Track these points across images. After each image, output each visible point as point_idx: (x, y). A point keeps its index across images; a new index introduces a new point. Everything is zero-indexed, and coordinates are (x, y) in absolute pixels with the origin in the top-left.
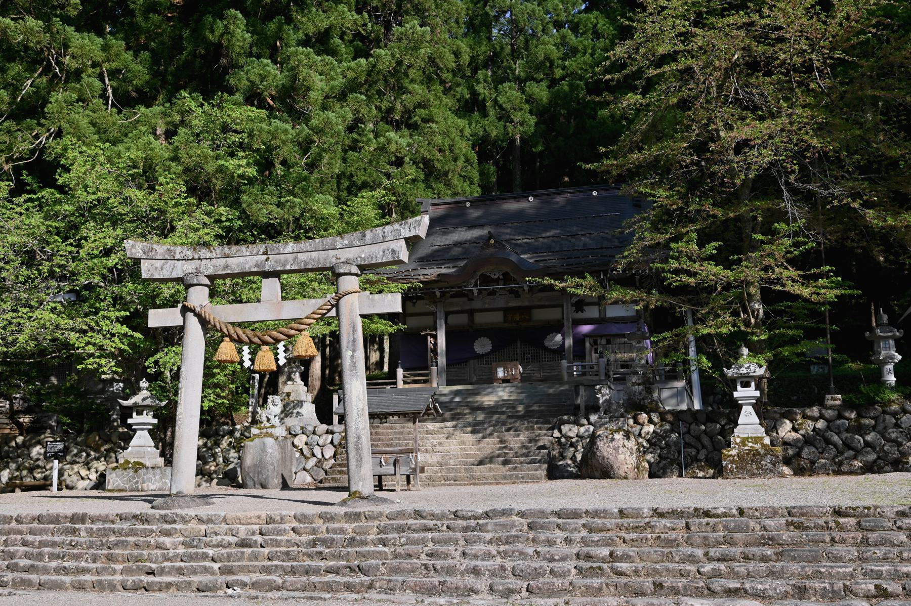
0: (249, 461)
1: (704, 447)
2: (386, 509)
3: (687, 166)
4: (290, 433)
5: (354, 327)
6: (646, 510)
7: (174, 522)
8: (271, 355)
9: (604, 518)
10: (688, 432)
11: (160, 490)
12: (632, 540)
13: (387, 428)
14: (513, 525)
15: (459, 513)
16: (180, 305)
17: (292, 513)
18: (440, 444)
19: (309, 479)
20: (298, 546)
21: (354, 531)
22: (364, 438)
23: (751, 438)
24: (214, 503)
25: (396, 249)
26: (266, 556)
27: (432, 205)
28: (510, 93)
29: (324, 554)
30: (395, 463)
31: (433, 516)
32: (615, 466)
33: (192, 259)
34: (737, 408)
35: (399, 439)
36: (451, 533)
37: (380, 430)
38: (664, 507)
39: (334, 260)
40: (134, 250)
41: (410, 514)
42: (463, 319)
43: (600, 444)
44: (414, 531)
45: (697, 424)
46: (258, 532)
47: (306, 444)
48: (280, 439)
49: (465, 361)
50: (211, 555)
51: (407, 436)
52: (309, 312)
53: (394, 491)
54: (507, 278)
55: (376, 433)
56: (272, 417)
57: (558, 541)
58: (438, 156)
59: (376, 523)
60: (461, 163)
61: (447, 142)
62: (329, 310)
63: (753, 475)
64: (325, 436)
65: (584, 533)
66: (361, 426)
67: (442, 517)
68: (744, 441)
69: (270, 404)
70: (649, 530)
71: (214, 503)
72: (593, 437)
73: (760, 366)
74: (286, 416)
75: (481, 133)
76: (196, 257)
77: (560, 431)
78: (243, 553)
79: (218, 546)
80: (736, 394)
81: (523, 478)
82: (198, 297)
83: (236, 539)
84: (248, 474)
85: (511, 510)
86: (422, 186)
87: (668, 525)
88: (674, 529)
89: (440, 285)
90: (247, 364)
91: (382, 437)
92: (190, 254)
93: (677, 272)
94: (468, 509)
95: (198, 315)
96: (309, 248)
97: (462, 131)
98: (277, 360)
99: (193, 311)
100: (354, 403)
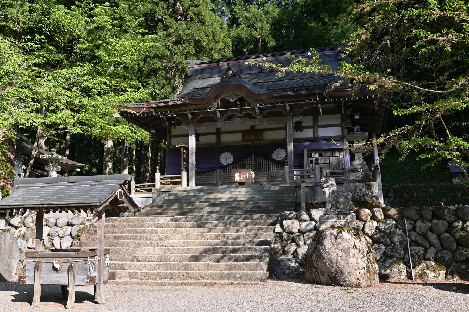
1: (431, 245)
10: (414, 229)
13: (124, 221)
27: (196, 64)
30: (70, 268)
32: (346, 272)
42: (212, 139)
43: (327, 242)
45: (422, 221)
49: (213, 170)
54: (242, 101)
55: (112, 225)
58: (205, 39)
61: (211, 30)
64: (64, 228)
72: (319, 238)
77: (282, 226)
89: (191, 107)
91: (116, 230)
93: (438, 25)
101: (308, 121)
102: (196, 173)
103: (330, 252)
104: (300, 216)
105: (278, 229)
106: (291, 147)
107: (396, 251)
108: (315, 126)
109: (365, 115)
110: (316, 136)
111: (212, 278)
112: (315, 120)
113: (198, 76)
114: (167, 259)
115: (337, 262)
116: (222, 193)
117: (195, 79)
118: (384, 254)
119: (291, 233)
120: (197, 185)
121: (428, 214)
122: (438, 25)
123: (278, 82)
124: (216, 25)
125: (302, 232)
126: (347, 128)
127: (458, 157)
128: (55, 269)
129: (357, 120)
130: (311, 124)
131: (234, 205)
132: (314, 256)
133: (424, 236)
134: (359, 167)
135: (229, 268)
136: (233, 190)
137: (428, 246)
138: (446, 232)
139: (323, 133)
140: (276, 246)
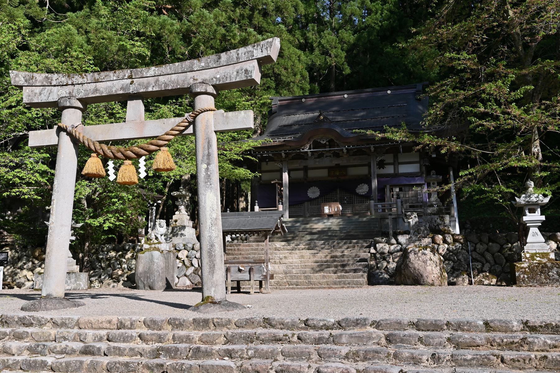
0: (140, 269)
1: (487, 261)
2: (235, 315)
3: (478, 44)
4: (176, 249)
5: (209, 142)
6: (515, 323)
7: (31, 325)
8: (133, 168)
9: (468, 330)
10: (475, 250)
11: (74, 289)
12: (513, 360)
13: (247, 246)
14: (370, 338)
15: (310, 322)
16: (56, 127)
17: (142, 319)
18: (285, 257)
19: (188, 283)
20: (141, 355)
21: (200, 340)
22: (216, 245)
23: (539, 253)
24: (84, 304)
25: (249, 69)
26: (104, 367)
27: (280, 101)
28: (329, 37)
29: (165, 366)
30: (250, 271)
31: (283, 325)
32: (424, 275)
33: (67, 85)
34: (525, 230)
35: (255, 254)
36: (303, 345)
37: (241, 247)
38: (535, 320)
39: (191, 81)
40: (17, 79)
41: (259, 322)
43: (412, 256)
44: (263, 342)
45: (481, 244)
46: (105, 338)
47: (187, 257)
48: (165, 252)
49: (302, 203)
50: (50, 363)
51: (261, 252)
52: (168, 129)
53: (249, 293)
54: (331, 143)
55: (238, 249)
56: (159, 236)
57: (425, 358)
58: (284, 72)
59: (225, 331)
60: (298, 77)
62: (187, 127)
63: (542, 284)
65: (450, 349)
66: (214, 234)
67: (292, 326)
68: (533, 256)
69: (158, 226)
70: (526, 347)
71: (84, 304)
72: (405, 253)
73: (545, 196)
74: (174, 236)
75: (310, 63)
76: (70, 82)
77: (375, 248)
78: (81, 363)
79: (61, 352)
80: (525, 218)
81: (349, 283)
82: (71, 118)
83: (82, 345)
84: (140, 278)
85: (365, 320)
86: (273, 92)
87: (549, 342)
88: (556, 347)
90: (112, 177)
91: (243, 252)
92: (64, 80)
93: (483, 116)
94: (319, 318)
95: (69, 134)
96: (169, 71)
97: (299, 57)
99: (65, 130)
100: (208, 213)
101: (389, 158)
102: (289, 206)
103: (414, 262)
104: (389, 241)
105: (373, 251)
106: (375, 183)
107: (462, 266)
108: (396, 163)
109: (438, 166)
110: (396, 172)
111: (328, 284)
112: (396, 157)
113: (283, 112)
114: (290, 272)
115: (418, 269)
116: (316, 223)
117: (280, 115)
118: (453, 268)
119: (382, 253)
120: (290, 217)
121: (485, 239)
122: (483, 116)
123: (360, 121)
124: (294, 58)
125: (390, 253)
126: (425, 165)
127: (501, 198)
128: (240, 270)
129: (434, 158)
130: (392, 161)
131: (330, 234)
132: (403, 266)
133: (482, 255)
134: (434, 203)
135: (339, 277)
136: (325, 221)
137: (485, 262)
138: (499, 252)
139: (403, 169)
140: (372, 263)
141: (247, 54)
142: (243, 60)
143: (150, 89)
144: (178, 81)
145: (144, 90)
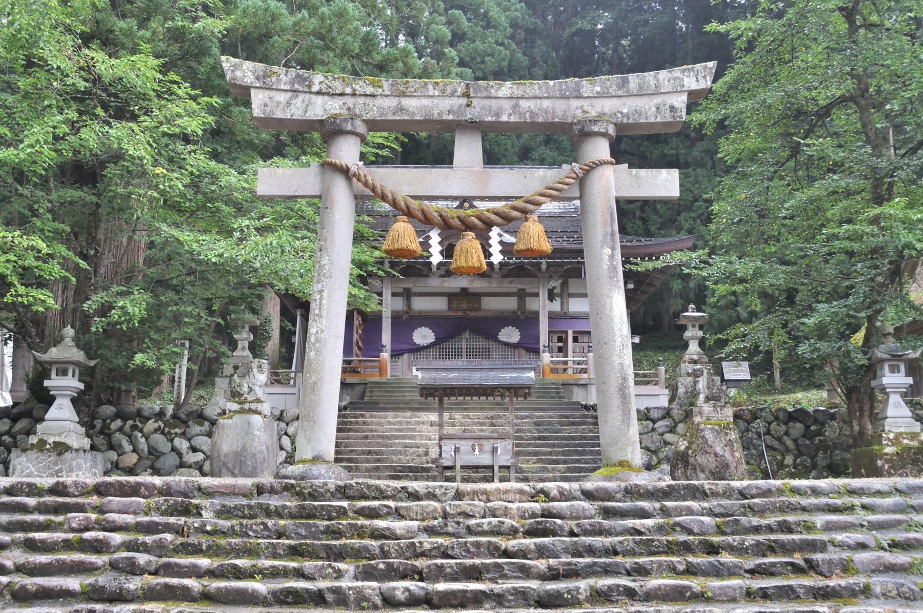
1: (788, 450)
10: (768, 433)
23: (906, 434)
39: (579, 113)
68: (898, 436)
76: (348, 90)
98: (487, 255)
110: (565, 310)
133: (779, 439)
141: (672, 82)
142: (666, 90)
143: (504, 118)
144: (554, 111)
145: (493, 119)
